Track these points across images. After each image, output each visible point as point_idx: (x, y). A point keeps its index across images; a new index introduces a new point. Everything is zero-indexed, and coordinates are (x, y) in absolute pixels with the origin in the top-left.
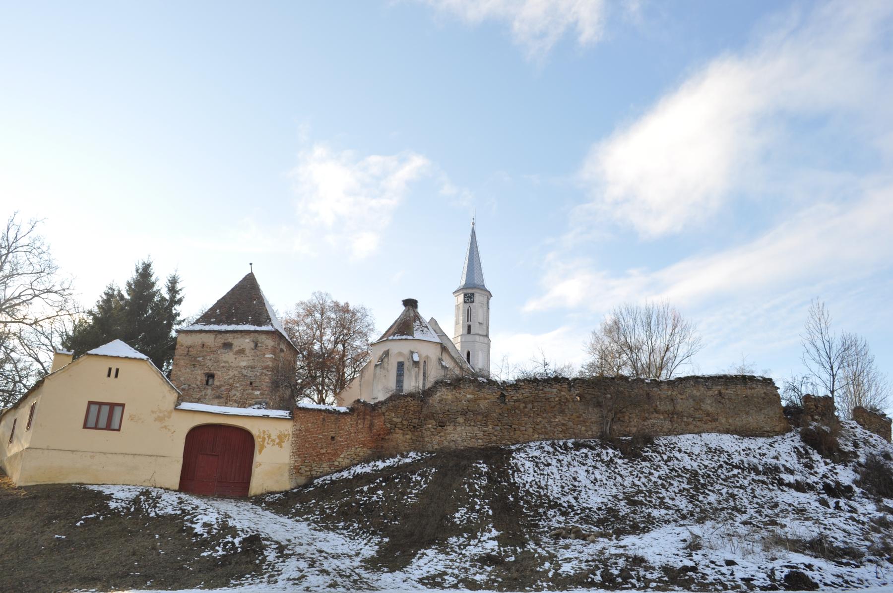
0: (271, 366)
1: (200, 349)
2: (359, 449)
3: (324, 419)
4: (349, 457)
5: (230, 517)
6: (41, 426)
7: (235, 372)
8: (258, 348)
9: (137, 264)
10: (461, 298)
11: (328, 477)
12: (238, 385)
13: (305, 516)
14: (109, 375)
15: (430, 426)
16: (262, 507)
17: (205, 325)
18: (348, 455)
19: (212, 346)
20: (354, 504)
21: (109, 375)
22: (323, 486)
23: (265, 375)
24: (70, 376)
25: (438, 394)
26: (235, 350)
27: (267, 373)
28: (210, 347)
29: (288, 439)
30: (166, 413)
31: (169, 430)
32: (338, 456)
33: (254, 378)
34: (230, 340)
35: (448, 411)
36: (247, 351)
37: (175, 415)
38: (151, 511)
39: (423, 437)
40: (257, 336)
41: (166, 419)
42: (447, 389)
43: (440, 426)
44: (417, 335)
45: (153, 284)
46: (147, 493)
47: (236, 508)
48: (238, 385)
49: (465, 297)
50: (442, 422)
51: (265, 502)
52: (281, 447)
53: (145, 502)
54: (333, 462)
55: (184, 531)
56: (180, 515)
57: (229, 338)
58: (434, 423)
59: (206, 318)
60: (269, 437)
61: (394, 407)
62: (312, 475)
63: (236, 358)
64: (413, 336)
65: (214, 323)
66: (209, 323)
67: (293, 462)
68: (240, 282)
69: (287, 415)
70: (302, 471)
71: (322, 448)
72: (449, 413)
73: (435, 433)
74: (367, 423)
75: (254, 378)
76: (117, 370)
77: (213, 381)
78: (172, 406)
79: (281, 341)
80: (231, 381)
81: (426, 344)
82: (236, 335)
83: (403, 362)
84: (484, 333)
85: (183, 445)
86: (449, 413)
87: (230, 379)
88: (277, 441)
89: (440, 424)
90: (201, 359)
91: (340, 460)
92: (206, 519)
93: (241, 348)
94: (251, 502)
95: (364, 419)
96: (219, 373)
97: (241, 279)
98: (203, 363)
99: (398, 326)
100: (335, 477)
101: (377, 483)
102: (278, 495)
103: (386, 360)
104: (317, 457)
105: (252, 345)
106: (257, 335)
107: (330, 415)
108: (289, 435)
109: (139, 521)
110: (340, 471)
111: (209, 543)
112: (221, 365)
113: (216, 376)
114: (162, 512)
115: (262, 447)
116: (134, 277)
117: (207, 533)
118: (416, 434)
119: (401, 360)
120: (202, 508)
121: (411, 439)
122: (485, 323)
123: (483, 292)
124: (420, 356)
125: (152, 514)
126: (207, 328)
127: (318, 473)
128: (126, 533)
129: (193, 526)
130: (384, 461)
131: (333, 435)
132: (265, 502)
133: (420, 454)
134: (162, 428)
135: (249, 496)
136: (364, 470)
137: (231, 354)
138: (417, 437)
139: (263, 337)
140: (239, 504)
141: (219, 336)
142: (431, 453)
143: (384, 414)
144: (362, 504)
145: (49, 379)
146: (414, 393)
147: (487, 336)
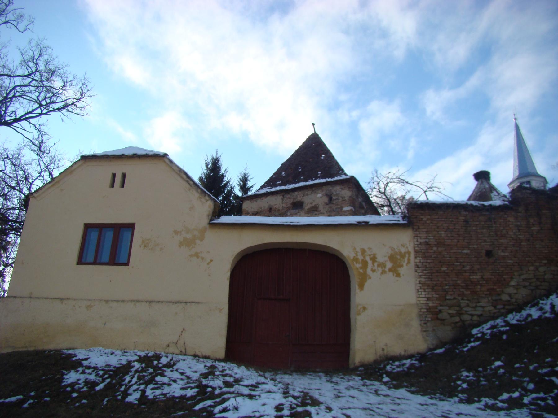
2: (542, 269)
3: (466, 221)
4: (527, 284)
5: (315, 403)
6: (23, 263)
8: (332, 202)
9: (206, 159)
11: (499, 321)
13: (505, 396)
14: (112, 185)
16: (385, 383)
17: (271, 188)
18: (524, 280)
19: (280, 208)
21: (112, 185)
24: (62, 190)
28: (279, 210)
29: (409, 260)
31: (203, 258)
34: (299, 199)
36: (321, 208)
37: (212, 235)
41: (198, 241)
45: (223, 176)
47: (330, 385)
51: (388, 374)
52: (398, 275)
53: (137, 371)
56: (192, 397)
57: (299, 196)
59: (271, 182)
60: (374, 259)
65: (280, 185)
67: (423, 301)
68: (304, 143)
69: (400, 219)
70: (444, 315)
76: (124, 176)
78: (206, 221)
82: (306, 192)
88: (389, 265)
93: (313, 205)
94: (359, 375)
100: (513, 318)
102: (408, 362)
105: (326, 200)
106: (330, 188)
108: (409, 253)
110: (519, 309)
115: (364, 278)
116: (205, 171)
120: (246, 382)
126: (274, 189)
127: (475, 318)
132: (388, 374)
135: (351, 366)
139: (337, 188)
140: (335, 379)
141: (287, 196)
145: (35, 198)
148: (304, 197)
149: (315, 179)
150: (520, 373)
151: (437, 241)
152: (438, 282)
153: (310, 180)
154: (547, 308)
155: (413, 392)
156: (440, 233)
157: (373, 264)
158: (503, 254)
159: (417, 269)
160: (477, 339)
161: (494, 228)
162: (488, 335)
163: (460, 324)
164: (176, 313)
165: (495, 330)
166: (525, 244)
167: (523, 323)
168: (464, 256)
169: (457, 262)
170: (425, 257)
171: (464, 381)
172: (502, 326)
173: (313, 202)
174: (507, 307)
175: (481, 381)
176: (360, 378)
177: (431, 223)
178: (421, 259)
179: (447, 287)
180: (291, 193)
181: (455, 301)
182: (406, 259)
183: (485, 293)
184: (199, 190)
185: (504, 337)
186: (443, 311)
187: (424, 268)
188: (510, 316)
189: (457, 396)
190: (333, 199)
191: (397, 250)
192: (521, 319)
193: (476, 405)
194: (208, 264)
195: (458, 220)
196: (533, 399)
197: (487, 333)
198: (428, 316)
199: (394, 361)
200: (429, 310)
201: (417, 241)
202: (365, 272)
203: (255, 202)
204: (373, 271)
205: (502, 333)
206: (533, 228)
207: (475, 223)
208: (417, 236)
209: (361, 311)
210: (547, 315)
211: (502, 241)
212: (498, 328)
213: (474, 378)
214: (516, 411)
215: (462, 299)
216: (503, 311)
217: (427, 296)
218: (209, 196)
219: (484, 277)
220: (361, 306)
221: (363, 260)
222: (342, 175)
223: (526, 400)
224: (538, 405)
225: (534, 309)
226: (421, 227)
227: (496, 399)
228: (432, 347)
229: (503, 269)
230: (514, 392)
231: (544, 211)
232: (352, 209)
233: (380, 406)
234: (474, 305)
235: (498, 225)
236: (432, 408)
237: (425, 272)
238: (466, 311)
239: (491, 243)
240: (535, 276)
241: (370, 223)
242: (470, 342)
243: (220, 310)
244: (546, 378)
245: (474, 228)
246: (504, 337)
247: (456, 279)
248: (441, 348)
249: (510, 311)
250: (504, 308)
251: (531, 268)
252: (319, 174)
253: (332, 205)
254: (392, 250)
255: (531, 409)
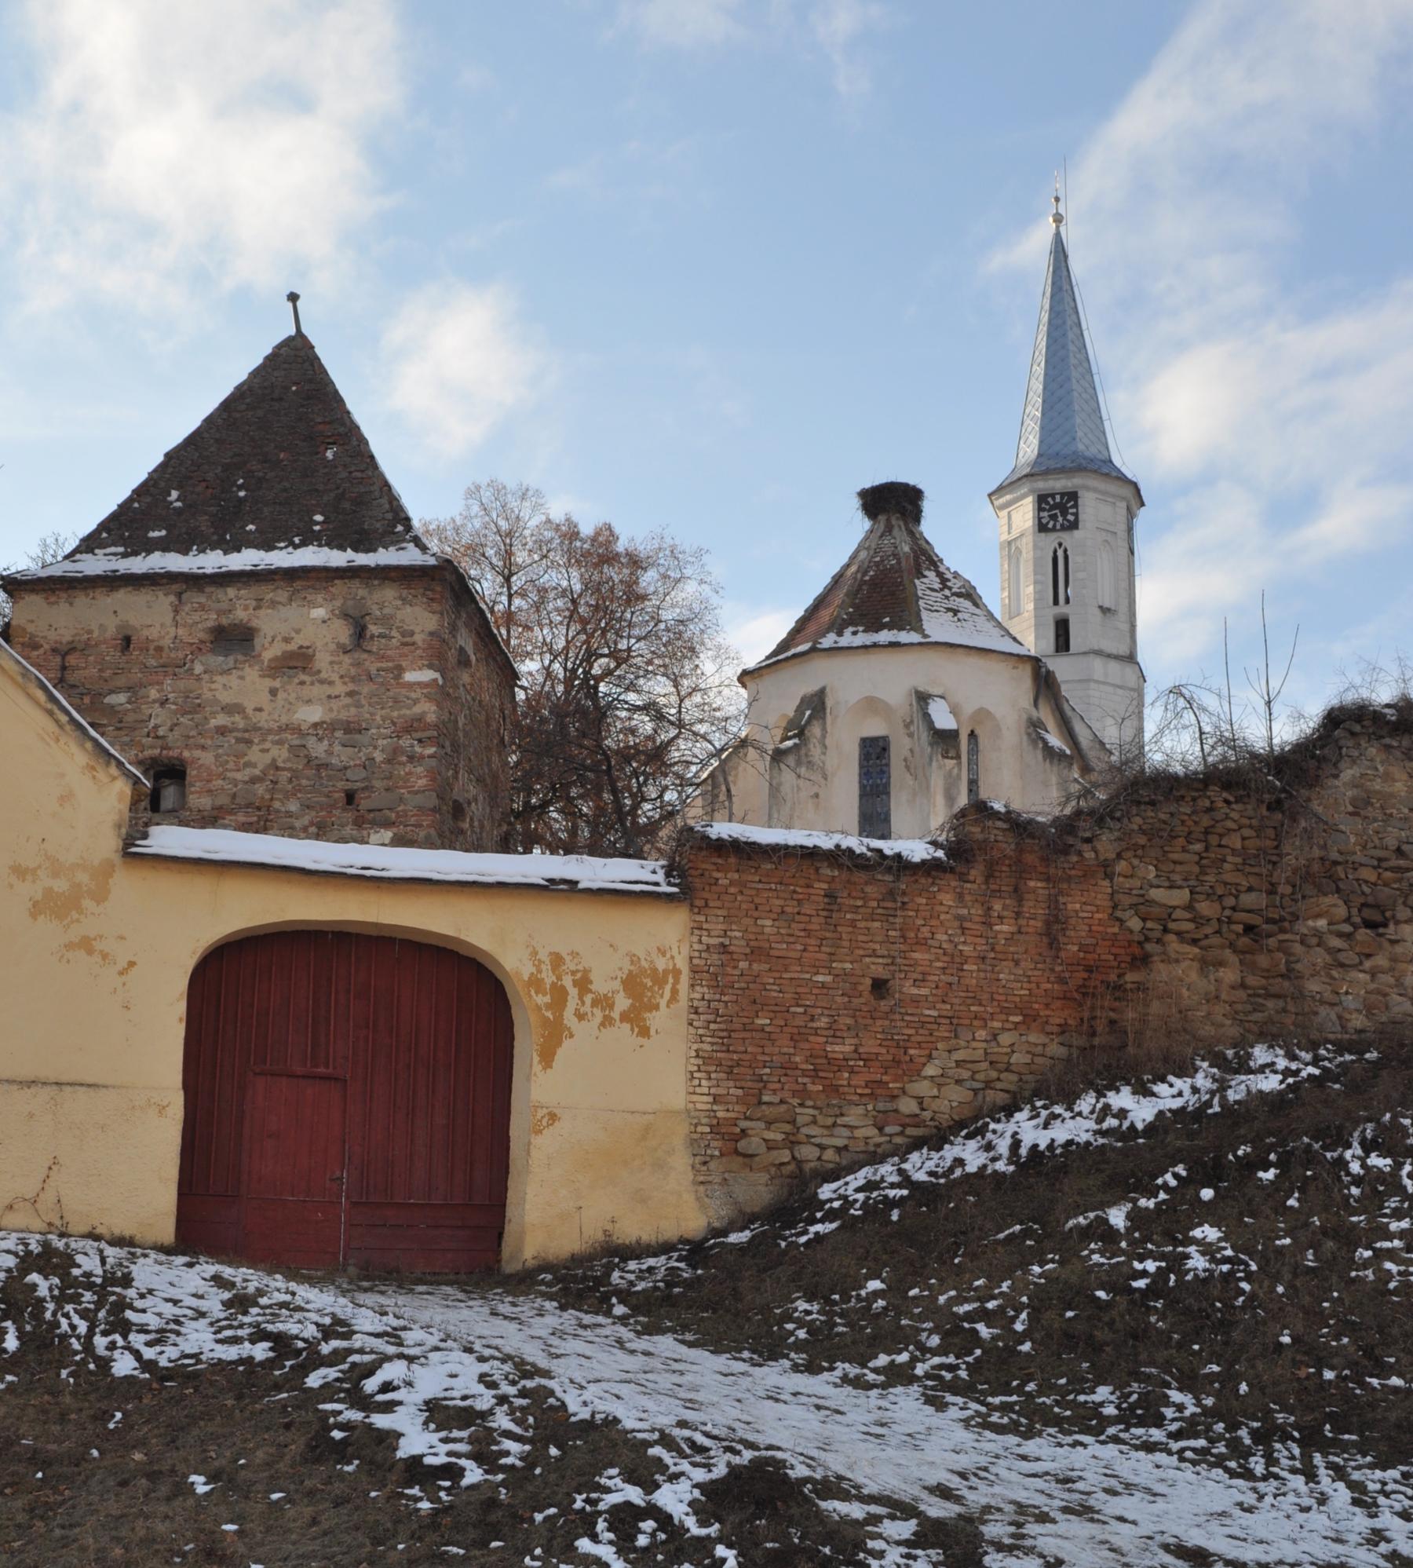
0: (431, 718)
1: (112, 656)
2: (1006, 1039)
3: (830, 896)
4: (966, 1074)
7: (275, 751)
8: (366, 645)
10: (1024, 514)
11: (887, 1171)
12: (293, 806)
13: (883, 1360)
15: (1322, 923)
17: (125, 555)
18: (958, 1063)
19: (167, 642)
20: (1101, 1294)
22: (876, 1211)
23: (411, 758)
25: (1348, 773)
26: (267, 655)
27: (418, 749)
28: (159, 649)
29: (674, 992)
30: (83, 877)
32: (917, 1074)
33: (363, 774)
34: (241, 615)
35: (1399, 852)
36: (322, 660)
37: (128, 884)
38: (112, 1346)
39: (1289, 974)
40: (362, 592)
41: (87, 903)
42: (1388, 747)
43: (1370, 925)
44: (937, 627)
46: (53, 1261)
48: (293, 806)
49: (1040, 509)
50: (1376, 906)
52: (644, 1032)
54: (894, 1097)
55: (342, 1451)
56: (268, 1364)
57: (240, 606)
58: (1341, 911)
60: (583, 983)
61: (1149, 833)
62: (799, 1163)
63: (273, 692)
64: (919, 629)
65: (164, 546)
66: (140, 546)
67: (703, 1102)
68: (255, 374)
69: (660, 877)
70: (753, 1144)
71: (835, 1036)
72: (1402, 863)
73: (1349, 957)
74: (1036, 911)
75: (363, 774)
77: (183, 795)
78: (109, 844)
79: (458, 617)
80: (260, 789)
81: (974, 661)
82: (268, 592)
83: (885, 739)
84: (1123, 650)
85: (179, 1031)
86: (1402, 863)
87: (254, 780)
88: (622, 1003)
89: (1368, 913)
90: (119, 699)
91: (923, 1088)
92: (430, 1382)
93: (292, 647)
95: (1018, 893)
96: (207, 758)
97: (258, 361)
98: (130, 718)
99: (853, 594)
100: (920, 1166)
101: (1165, 1187)
103: (816, 730)
104: (815, 1075)
105: (343, 632)
107: (860, 877)
108: (677, 973)
109: (68, 1399)
110: (937, 1140)
111: (518, 1517)
112: (213, 723)
113: (191, 773)
114: (172, 1352)
115: (554, 1036)
117: (478, 1457)
118: (1263, 960)
119: (875, 728)
121: (1243, 985)
122: (1123, 609)
123: (1113, 487)
124: (955, 711)
125: (124, 1366)
126: (138, 565)
127: (829, 1155)
128: (21, 1468)
129: (380, 1421)
130: (1143, 1091)
131: (880, 972)
132: (625, 1296)
133: (1307, 1056)
134: (70, 946)
135: (509, 1267)
136: (1060, 1133)
137: (252, 673)
138: (1267, 974)
139: (389, 594)
141: (195, 598)
142: (1357, 1047)
143: (1106, 869)
144: (1145, 1293)
146: (1238, 770)
147: (1131, 658)
148: (262, 612)
149: (304, 544)
150: (917, 1311)
151: (752, 943)
152: (743, 1056)
153: (282, 545)
154: (1003, 1146)
155: (690, 1345)
156: (759, 922)
157: (581, 998)
158: (915, 991)
159: (693, 1016)
160: (830, 1216)
161: (897, 920)
162: (858, 1205)
163: (792, 1167)
164: (31, 1115)
165: (875, 1194)
166: (975, 967)
167: (942, 1181)
168: (815, 991)
169: (798, 1005)
170: (715, 987)
171: (801, 1323)
172: (893, 1186)
173: (293, 634)
174: (909, 1131)
175: (836, 1325)
176: (555, 1304)
177: (741, 892)
178: (706, 990)
179: (767, 1071)
180: (208, 589)
181: (783, 1108)
182: (668, 988)
183: (859, 1091)
184: (89, 745)
185: (895, 1216)
186: (750, 1132)
187: (711, 1017)
188: (915, 1157)
189: (787, 1357)
190: (368, 635)
191: (644, 964)
192: (940, 1170)
193: (826, 1376)
194: (121, 973)
195: (811, 891)
196: (933, 1368)
197: (856, 1201)
198: (714, 1144)
199: (624, 1260)
200: (716, 1128)
201: (700, 942)
202: (559, 1018)
203: (64, 606)
204: (581, 1017)
205: (891, 1203)
206: (997, 928)
207: (852, 902)
208: (701, 929)
209: (544, 1122)
210: (1001, 1166)
211: (916, 955)
212: (883, 1189)
213: (822, 1318)
214: (899, 1389)
215: (801, 1105)
216: (898, 1140)
217: (713, 1091)
218: (120, 764)
219: (861, 1050)
220: (545, 1111)
221: (553, 985)
222: (404, 545)
223: (920, 1370)
224: (940, 1378)
225: (973, 1144)
226: (711, 904)
227: (864, 1366)
228: (717, 1224)
229: (912, 1032)
230: (899, 1352)
231: (1032, 884)
232: (435, 680)
233: (649, 1376)
234: (830, 1121)
235: (911, 913)
236: (745, 1382)
237: (712, 1026)
238: (809, 1136)
239: (889, 961)
240: (986, 1054)
241: (581, 886)
242: (814, 1221)
243: (162, 1109)
244: (966, 1325)
245: (848, 916)
246: (895, 1216)
247: (792, 1051)
248: (742, 1230)
249: (917, 1145)
250: (902, 1133)
251: (981, 1034)
252: (317, 523)
253: (365, 656)
254: (632, 962)
255: (925, 1387)
